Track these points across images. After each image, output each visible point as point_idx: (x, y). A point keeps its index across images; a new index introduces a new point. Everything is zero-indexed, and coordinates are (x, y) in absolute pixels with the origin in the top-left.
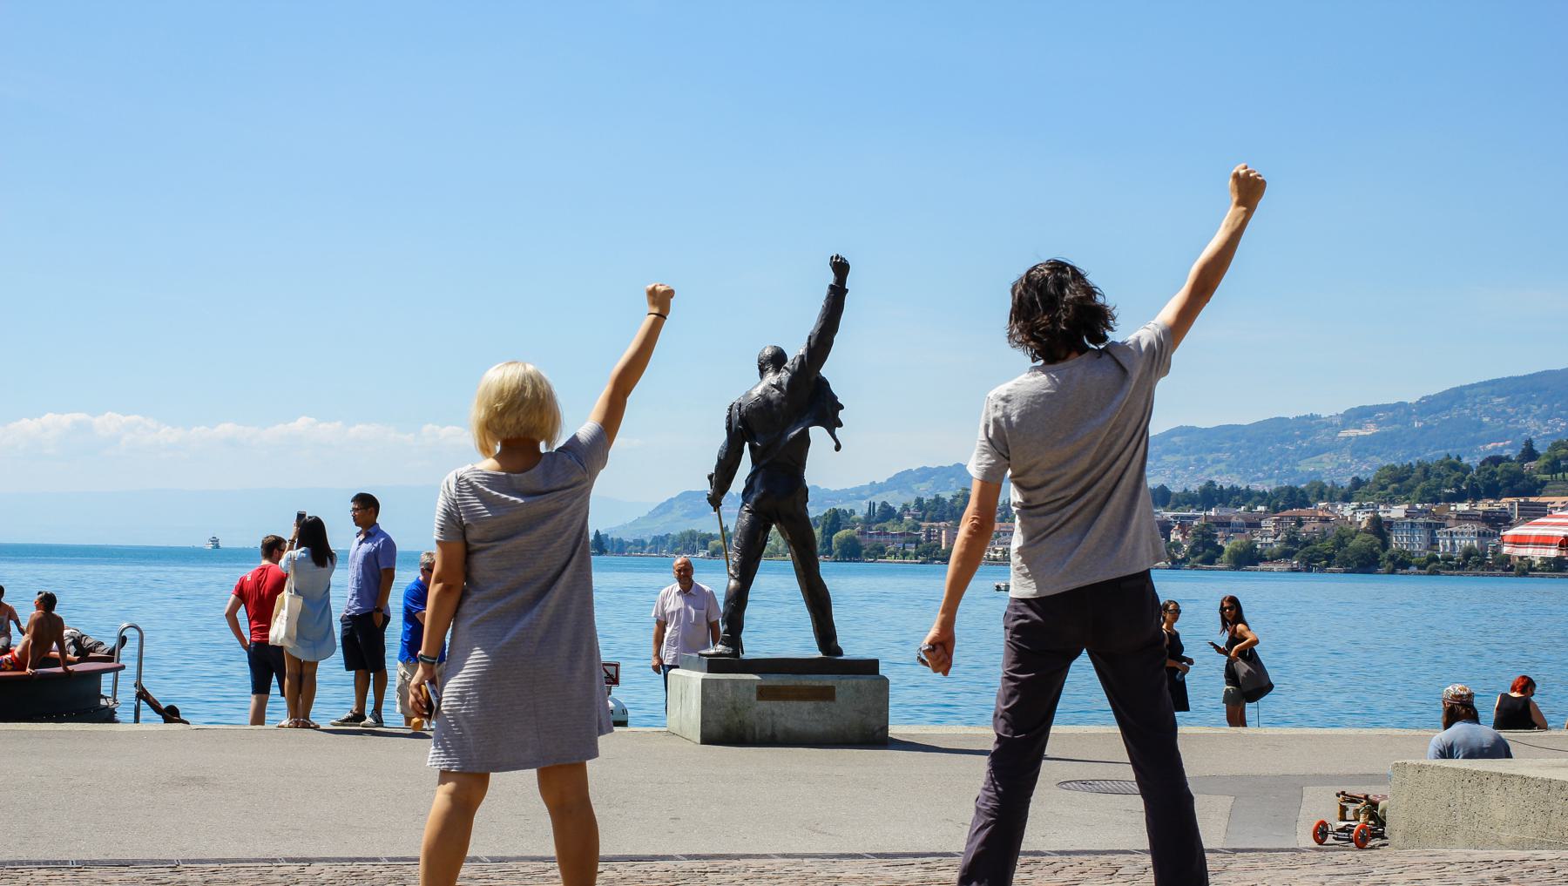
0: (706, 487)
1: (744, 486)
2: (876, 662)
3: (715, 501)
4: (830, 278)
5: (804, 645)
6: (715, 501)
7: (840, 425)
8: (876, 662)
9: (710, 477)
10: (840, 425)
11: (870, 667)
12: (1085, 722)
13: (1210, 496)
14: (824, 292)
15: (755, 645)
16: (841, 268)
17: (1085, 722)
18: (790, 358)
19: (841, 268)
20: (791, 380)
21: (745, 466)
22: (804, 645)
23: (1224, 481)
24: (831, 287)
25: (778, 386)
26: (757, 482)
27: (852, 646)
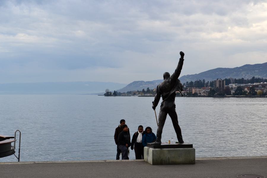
0: (152, 105)
1: (161, 105)
2: (192, 145)
3: (154, 108)
4: (180, 57)
5: (174, 140)
6: (154, 108)
7: (166, 75)
8: (192, 145)
9: (153, 102)
10: (166, 75)
11: (191, 146)
12: (168, 118)
13: (254, 80)
14: (178, 61)
15: (164, 141)
16: (182, 54)
17: (168, 118)
18: (171, 75)
19: (182, 54)
20: (171, 80)
21: (161, 100)
22: (174, 140)
23: (257, 77)
24: (180, 59)
25: (168, 82)
26: (164, 103)
27: (186, 141)
